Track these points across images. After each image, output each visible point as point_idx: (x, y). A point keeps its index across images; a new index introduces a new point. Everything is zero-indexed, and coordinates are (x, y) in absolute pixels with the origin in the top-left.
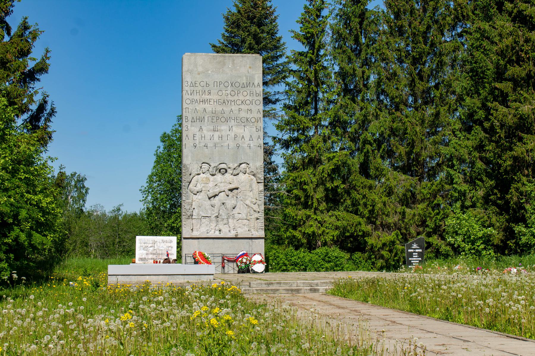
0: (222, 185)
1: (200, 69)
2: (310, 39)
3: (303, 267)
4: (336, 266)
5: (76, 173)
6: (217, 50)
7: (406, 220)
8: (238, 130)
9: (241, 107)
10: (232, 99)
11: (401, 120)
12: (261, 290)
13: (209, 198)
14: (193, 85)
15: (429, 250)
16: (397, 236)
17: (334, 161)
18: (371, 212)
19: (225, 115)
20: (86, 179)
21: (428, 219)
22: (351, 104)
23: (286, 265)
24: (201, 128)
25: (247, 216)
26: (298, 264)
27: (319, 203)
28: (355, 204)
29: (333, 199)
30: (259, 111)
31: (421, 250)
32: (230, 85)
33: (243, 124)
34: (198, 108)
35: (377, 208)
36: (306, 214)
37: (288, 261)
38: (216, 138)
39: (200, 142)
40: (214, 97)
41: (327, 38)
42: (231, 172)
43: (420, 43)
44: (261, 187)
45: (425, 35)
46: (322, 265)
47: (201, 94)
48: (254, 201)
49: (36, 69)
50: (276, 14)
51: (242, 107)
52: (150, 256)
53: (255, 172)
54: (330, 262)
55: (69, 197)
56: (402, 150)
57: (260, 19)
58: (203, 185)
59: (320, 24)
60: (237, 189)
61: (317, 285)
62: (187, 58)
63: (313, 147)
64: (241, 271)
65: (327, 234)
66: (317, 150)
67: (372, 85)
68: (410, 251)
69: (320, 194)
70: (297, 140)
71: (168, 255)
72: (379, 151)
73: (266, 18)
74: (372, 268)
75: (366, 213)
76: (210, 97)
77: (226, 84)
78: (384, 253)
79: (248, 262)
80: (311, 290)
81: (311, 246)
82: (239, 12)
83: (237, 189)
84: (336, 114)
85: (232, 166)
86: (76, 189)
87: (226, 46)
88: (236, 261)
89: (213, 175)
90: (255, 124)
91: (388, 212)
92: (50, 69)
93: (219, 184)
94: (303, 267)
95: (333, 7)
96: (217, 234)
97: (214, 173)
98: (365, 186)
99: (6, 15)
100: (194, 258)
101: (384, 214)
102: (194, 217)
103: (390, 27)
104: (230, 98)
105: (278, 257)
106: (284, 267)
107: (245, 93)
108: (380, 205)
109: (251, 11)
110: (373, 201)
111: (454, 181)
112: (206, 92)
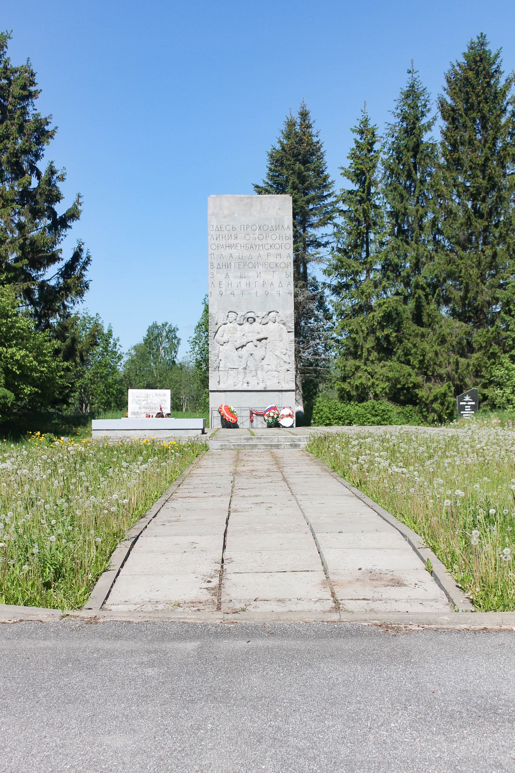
0: (250, 334)
1: (226, 212)
2: (360, 176)
3: (348, 421)
4: (384, 420)
5: (167, 323)
6: (260, 190)
7: (459, 371)
8: (267, 277)
9: (269, 251)
10: (260, 243)
11: (454, 262)
12: (238, 445)
13: (237, 349)
14: (219, 229)
15: (485, 403)
16: (449, 387)
17: (384, 308)
18: (421, 362)
19: (252, 261)
20: (177, 329)
21: (484, 369)
22: (403, 245)
23: (330, 419)
24: (227, 275)
25: (277, 367)
26: (342, 418)
27: (369, 352)
28: (407, 353)
29: (385, 350)
30: (289, 256)
31: (474, 403)
32: (258, 228)
33: (272, 270)
34: (224, 254)
35: (427, 358)
36: (355, 365)
37: (332, 415)
38: (243, 286)
39: (226, 290)
40: (241, 241)
41: (379, 174)
42: (260, 321)
43: (478, 177)
44: (292, 336)
45: (484, 166)
46: (369, 419)
47: (227, 238)
48: (284, 351)
49: (67, 215)
50: (322, 150)
51: (271, 251)
52: (143, 410)
53: (285, 321)
54: (377, 415)
55: (161, 348)
56: (457, 294)
57: (304, 156)
58: (230, 335)
59: (372, 160)
60: (266, 339)
61: (299, 440)
62: (213, 201)
63: (363, 293)
64: (270, 426)
65: (377, 385)
66: (366, 296)
67: (427, 225)
68: (461, 403)
69: (370, 343)
70: (347, 286)
71: (161, 409)
72: (433, 296)
73: (312, 154)
74: (422, 422)
75: (416, 363)
76: (237, 242)
77: (254, 228)
78: (436, 406)
79: (275, 416)
80: (291, 445)
81: (362, 398)
82: (283, 149)
83: (266, 339)
84: (386, 256)
85: (261, 314)
86: (167, 340)
87: (271, 186)
88: (263, 415)
89: (240, 325)
90: (285, 269)
91: (441, 362)
92: (81, 216)
93: (246, 334)
94: (348, 421)
95: (385, 140)
96: (245, 387)
97: (241, 322)
98: (417, 335)
99: (37, 160)
100: (220, 412)
101: (435, 364)
102: (220, 369)
103: (447, 160)
104: (258, 242)
105: (322, 410)
106: (328, 422)
107: (274, 237)
108: (431, 355)
109: (295, 147)
110: (423, 350)
111: (510, 328)
112: (233, 236)
